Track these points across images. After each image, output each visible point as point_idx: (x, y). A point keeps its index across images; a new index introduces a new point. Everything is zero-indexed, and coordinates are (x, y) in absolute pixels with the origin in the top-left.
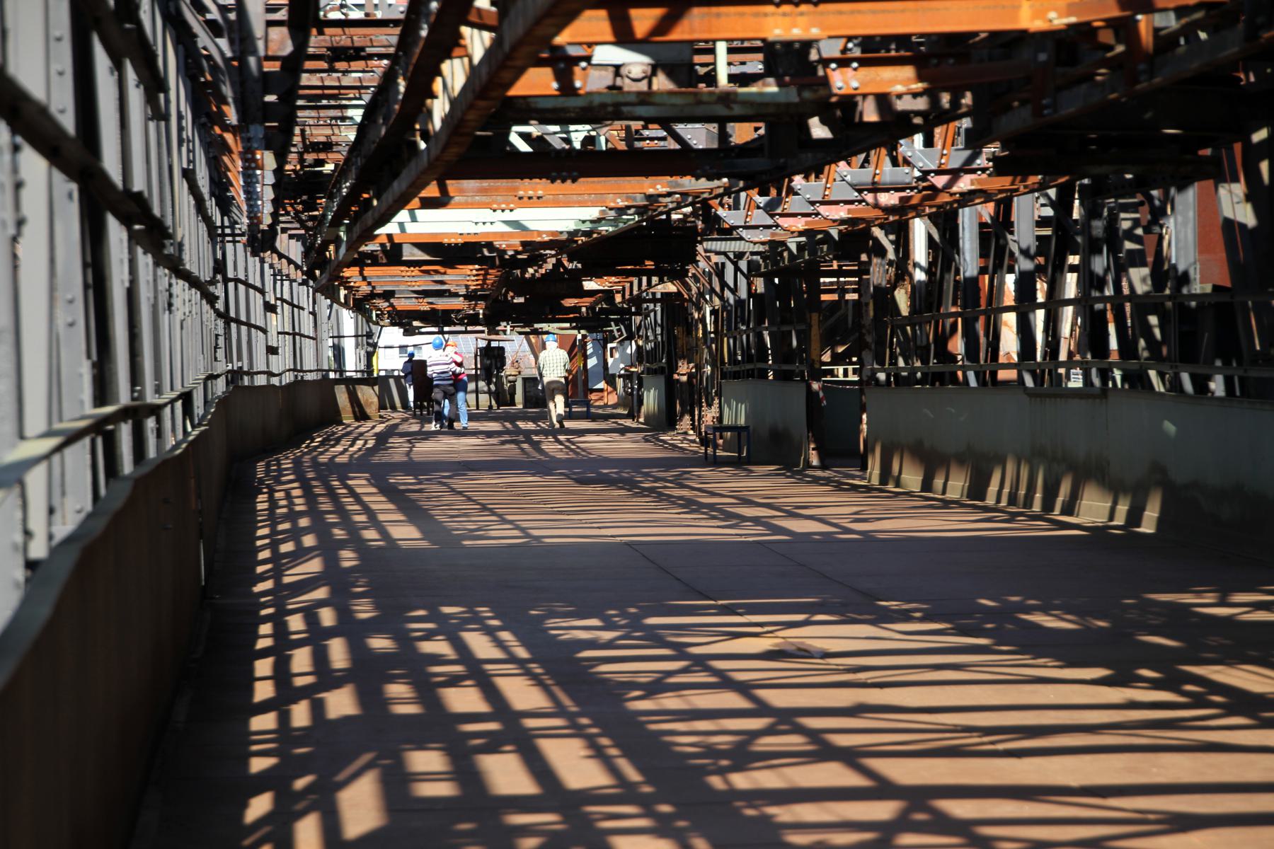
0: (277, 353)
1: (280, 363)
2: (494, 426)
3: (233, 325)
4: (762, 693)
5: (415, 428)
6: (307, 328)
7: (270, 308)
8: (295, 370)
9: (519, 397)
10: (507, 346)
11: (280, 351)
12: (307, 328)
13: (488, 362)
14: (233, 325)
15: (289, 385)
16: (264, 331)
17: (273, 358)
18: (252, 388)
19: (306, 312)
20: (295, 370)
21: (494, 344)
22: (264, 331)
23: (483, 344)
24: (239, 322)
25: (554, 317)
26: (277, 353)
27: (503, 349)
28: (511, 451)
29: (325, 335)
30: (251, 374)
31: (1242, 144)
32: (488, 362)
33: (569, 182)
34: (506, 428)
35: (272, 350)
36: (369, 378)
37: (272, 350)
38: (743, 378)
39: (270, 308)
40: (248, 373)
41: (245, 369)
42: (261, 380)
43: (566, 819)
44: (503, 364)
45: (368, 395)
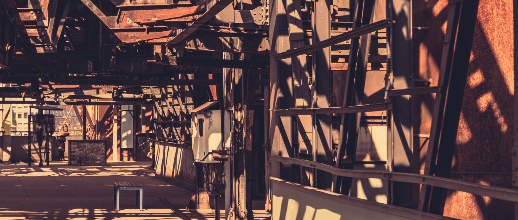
13: (40, 127)
32: (40, 127)
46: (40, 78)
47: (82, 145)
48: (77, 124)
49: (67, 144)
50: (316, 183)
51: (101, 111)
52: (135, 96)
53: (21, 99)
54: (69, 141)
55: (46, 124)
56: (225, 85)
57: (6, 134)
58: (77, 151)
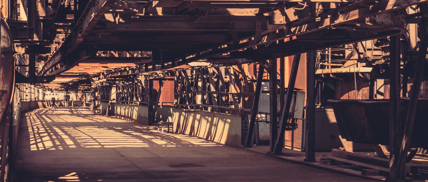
0: (27, 96)
1: (28, 98)
2: (69, 109)
3: (21, 92)
4: (93, 137)
5: (54, 109)
6: (33, 92)
7: (27, 88)
8: (30, 99)
9: (73, 105)
10: (70, 95)
11: (28, 96)
12: (33, 92)
13: (67, 98)
14: (21, 92)
15: (29, 102)
16: (26, 92)
17: (27, 97)
18: (23, 102)
19: (33, 89)
20: (30, 99)
21: (68, 95)
22: (26, 92)
23: (66, 94)
24: (22, 91)
25: (77, 3)
26: (27, 96)
27: (69, 95)
28: (70, 113)
29: (36, 93)
30: (23, 99)
31: (412, 48)
32: (67, 98)
33: (105, 64)
34: (78, 113)
35: (27, 96)
36: (43, 101)
37: (27, 96)
38: (225, 71)
39: (27, 88)
40: (23, 99)
41: (22, 99)
42: (25, 101)
43: (56, 148)
44: (69, 98)
45: (46, 103)
46: (410, 99)
47: (76, 102)
48: (342, 17)
49: (73, 102)
50: (106, 90)
51: (81, 94)
52: (194, 75)
53: (62, 92)
54: (73, 101)
55: (68, 97)
56: (381, 160)
57: (58, 100)
58: (75, 103)
